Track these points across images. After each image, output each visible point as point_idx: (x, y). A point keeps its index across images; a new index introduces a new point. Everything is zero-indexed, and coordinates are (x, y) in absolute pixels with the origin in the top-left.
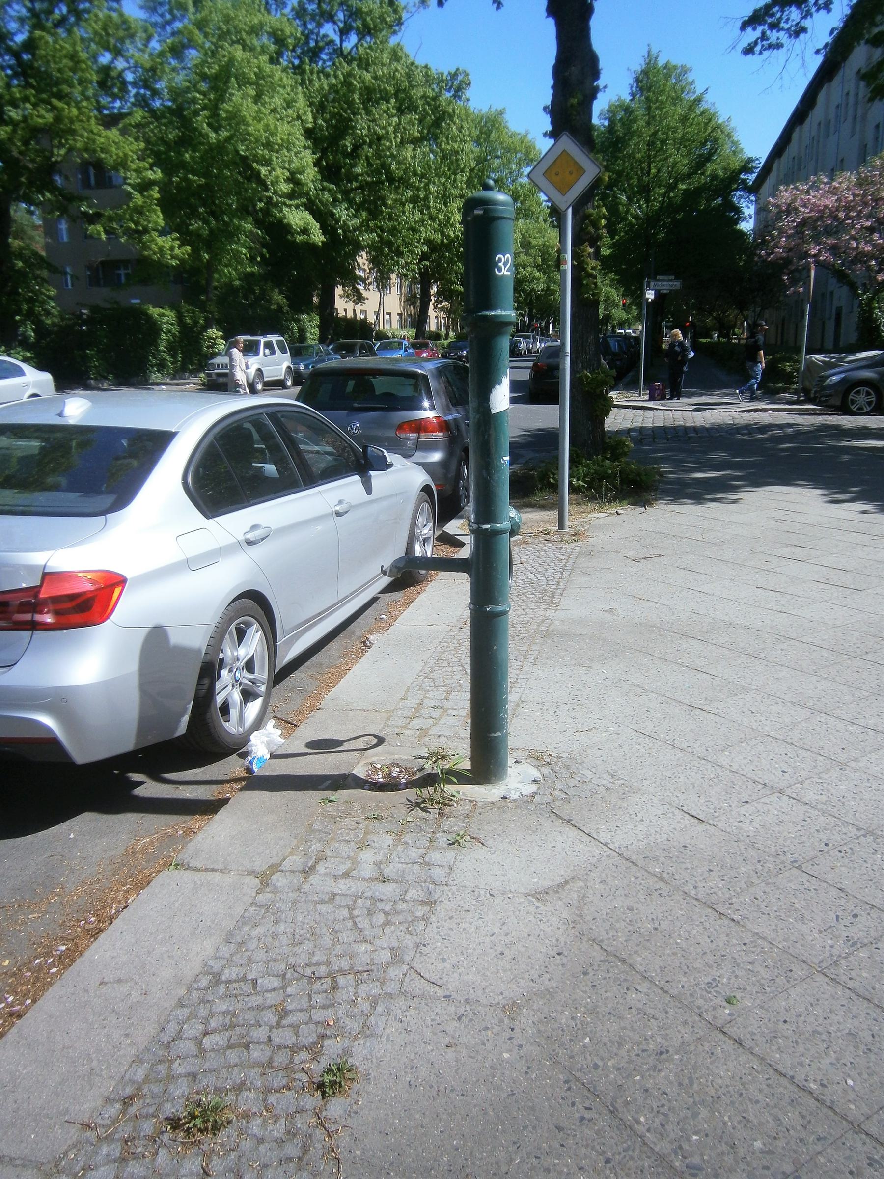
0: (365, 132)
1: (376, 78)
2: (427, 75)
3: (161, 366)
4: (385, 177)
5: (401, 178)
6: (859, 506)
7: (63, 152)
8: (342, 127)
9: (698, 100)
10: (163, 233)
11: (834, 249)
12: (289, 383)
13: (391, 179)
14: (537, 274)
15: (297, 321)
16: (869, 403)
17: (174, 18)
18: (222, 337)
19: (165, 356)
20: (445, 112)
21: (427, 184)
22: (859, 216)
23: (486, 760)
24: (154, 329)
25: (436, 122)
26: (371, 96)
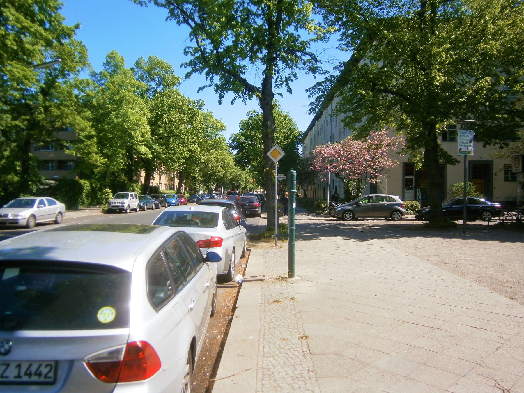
0: (166, 119)
1: (173, 102)
2: (189, 101)
3: (83, 203)
4: (171, 134)
5: (178, 135)
6: (352, 240)
7: (59, 124)
8: (158, 118)
9: (286, 116)
10: (97, 154)
11: (335, 167)
12: (138, 210)
13: (174, 136)
14: (221, 170)
15: (132, 186)
16: (351, 217)
17: (102, 80)
18: (111, 192)
19: (85, 199)
20: (195, 114)
21: (188, 138)
22: (342, 157)
23: (291, 273)
24: (81, 188)
25: (192, 116)
26: (170, 108)
